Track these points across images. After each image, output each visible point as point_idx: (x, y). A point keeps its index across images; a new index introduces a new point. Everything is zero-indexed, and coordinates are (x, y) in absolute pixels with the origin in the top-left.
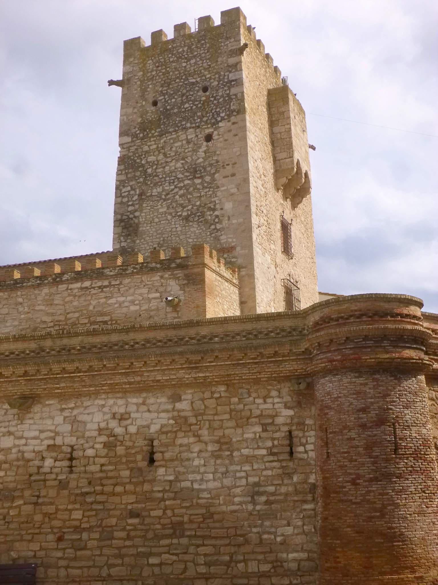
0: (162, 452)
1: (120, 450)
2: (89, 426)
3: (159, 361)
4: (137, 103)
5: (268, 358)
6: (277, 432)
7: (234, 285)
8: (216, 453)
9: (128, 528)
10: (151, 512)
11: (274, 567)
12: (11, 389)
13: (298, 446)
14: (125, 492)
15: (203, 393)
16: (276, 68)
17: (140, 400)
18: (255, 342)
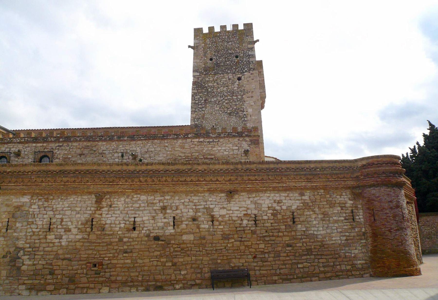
1: (279, 217)
2: (263, 206)
4: (202, 58)
9: (287, 251)
11: (352, 267)
14: (284, 236)
15: (314, 192)
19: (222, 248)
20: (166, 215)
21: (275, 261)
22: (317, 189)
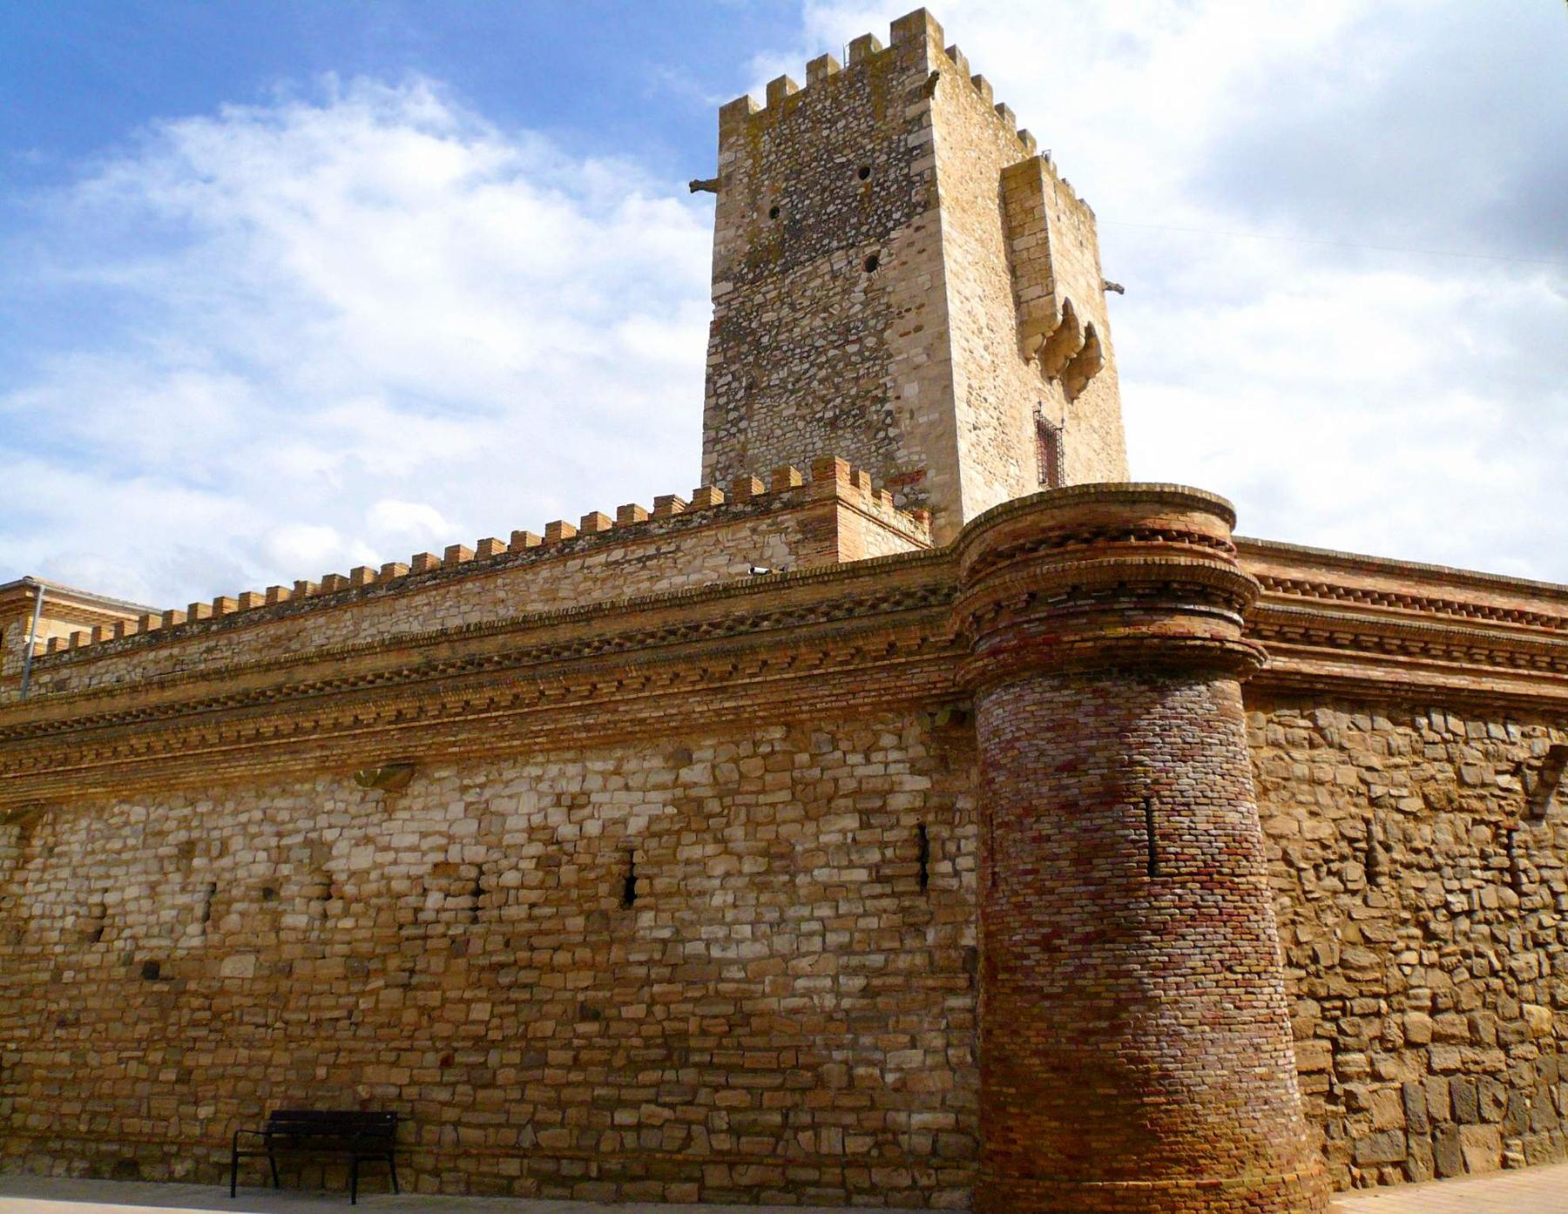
0: (650, 878)
1: (568, 873)
2: (511, 823)
3: (648, 679)
5: (876, 659)
6: (892, 828)
8: (758, 879)
9: (576, 1042)
10: (624, 1009)
11: (877, 1145)
13: (938, 861)
14: (576, 965)
19: (336, 1014)
20: (192, 879)
21: (523, 1085)
22: (750, 725)
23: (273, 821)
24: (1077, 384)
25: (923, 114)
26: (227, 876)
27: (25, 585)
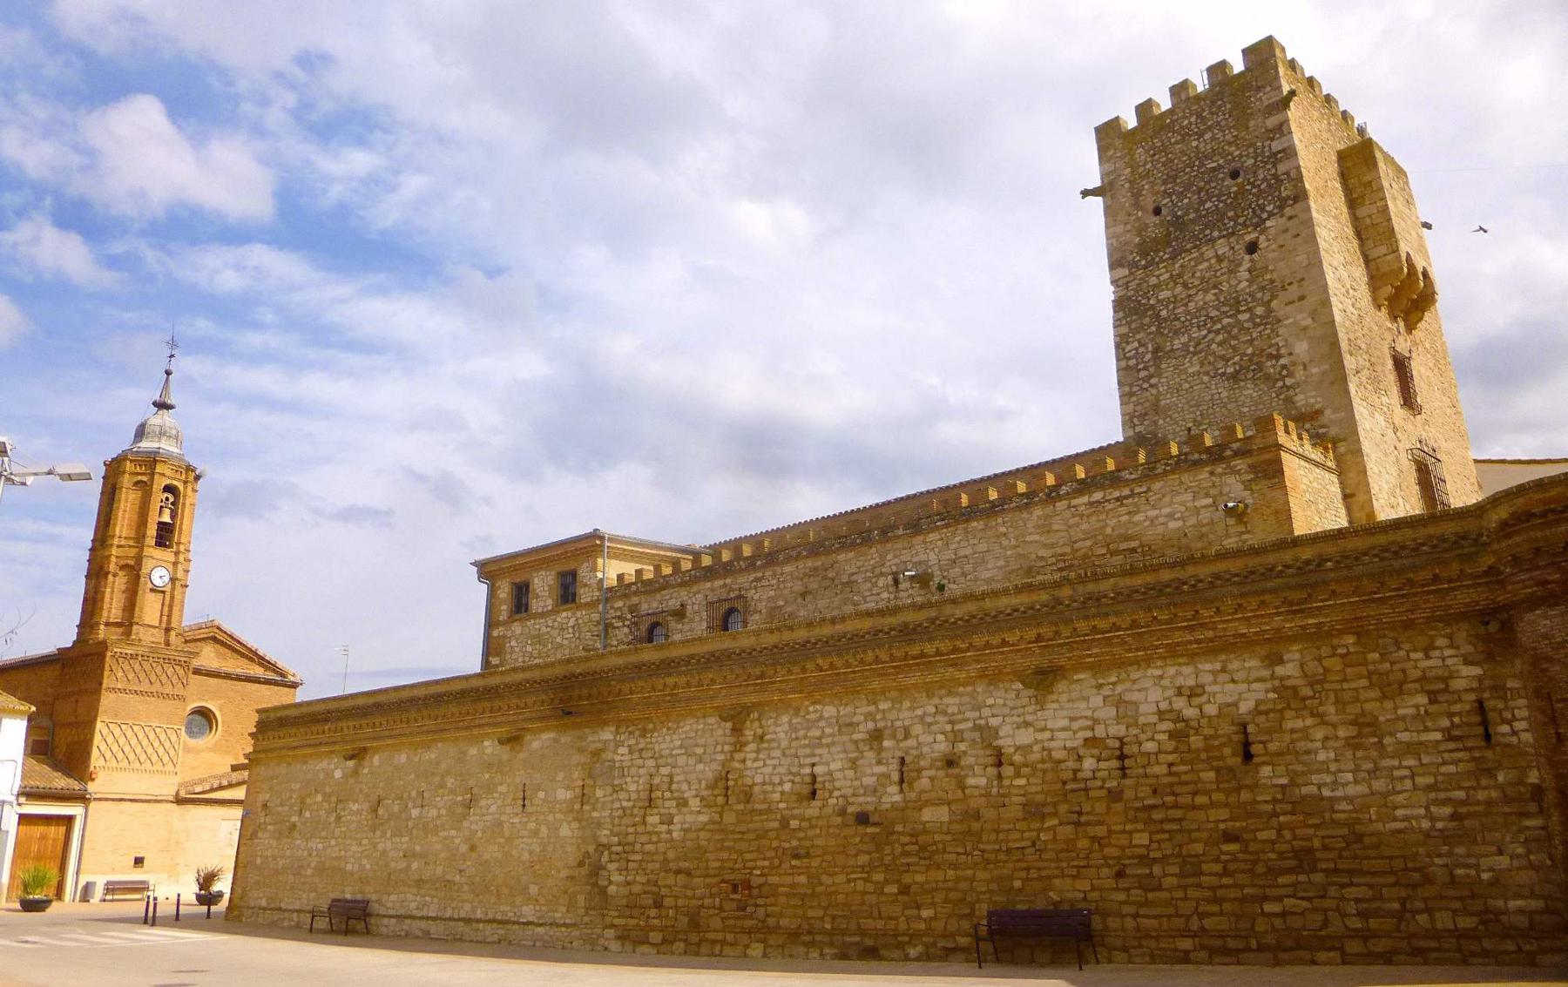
1: (1195, 741)
2: (1143, 708)
7: (1329, 470)
11: (1482, 922)
12: (1021, 662)
14: (1212, 805)
16: (1344, 113)
17: (1218, 666)
18: (1397, 564)
19: (1023, 844)
20: (884, 755)
21: (1185, 888)
22: (1329, 634)
23: (945, 713)
24: (1413, 317)
25: (1281, 125)
26: (914, 752)
27: (595, 535)
